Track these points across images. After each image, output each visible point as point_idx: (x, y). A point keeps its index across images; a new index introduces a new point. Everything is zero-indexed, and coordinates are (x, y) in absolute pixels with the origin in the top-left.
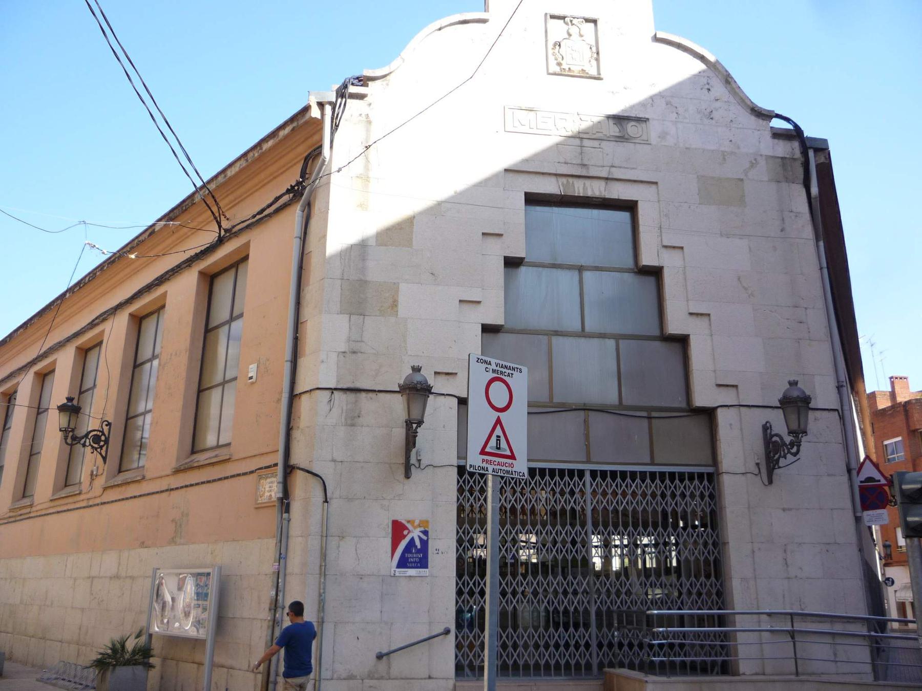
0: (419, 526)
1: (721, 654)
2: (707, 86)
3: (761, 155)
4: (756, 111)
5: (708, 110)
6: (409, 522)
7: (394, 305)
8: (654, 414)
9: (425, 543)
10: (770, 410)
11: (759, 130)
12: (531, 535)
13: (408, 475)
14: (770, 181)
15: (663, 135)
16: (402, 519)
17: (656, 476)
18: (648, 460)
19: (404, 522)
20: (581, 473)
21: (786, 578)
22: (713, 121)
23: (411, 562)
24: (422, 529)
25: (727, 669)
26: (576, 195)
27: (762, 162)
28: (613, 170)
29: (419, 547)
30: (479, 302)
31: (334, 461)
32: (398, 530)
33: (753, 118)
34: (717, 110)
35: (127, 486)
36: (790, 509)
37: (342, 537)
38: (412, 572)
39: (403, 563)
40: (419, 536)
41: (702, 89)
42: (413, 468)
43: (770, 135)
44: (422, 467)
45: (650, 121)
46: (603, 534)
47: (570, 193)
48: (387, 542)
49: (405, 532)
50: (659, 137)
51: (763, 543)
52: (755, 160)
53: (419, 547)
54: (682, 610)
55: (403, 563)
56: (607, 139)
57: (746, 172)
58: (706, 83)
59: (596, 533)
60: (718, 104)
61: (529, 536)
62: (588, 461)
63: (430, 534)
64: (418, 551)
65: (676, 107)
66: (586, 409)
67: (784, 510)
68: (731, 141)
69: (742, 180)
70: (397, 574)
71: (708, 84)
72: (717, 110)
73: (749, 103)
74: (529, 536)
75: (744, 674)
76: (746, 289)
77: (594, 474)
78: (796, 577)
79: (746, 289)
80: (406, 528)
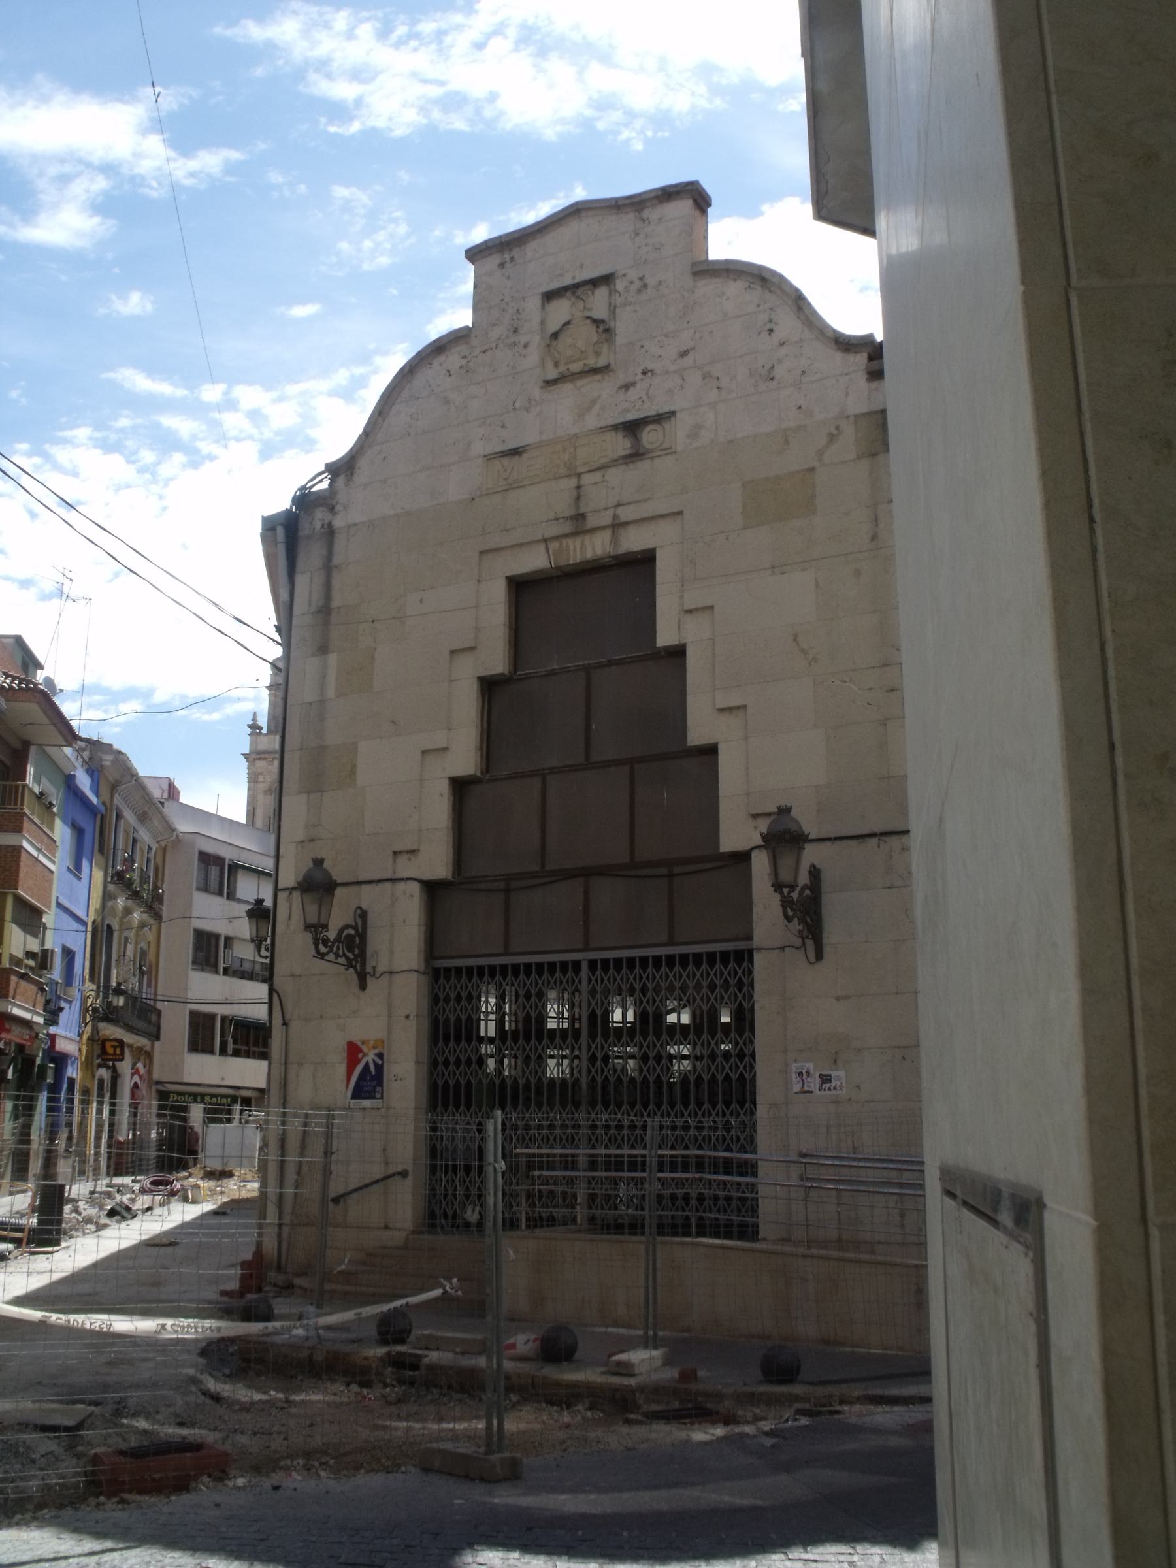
0: (374, 1047)
1: (725, 1211)
2: (768, 326)
3: (848, 417)
4: (841, 343)
5: (767, 367)
6: (363, 1043)
7: (353, 772)
8: (677, 870)
9: (379, 1068)
10: (828, 843)
11: (847, 374)
12: (682, 1047)
13: (363, 987)
14: (859, 458)
15: (694, 434)
16: (356, 1038)
17: (688, 960)
18: (664, 938)
19: (359, 1044)
20: (577, 965)
21: (834, 1102)
22: (775, 383)
23: (366, 1092)
24: (376, 1051)
25: (748, 1232)
26: (571, 562)
27: (849, 431)
28: (620, 511)
29: (374, 1073)
30: (446, 749)
31: (293, 975)
32: (353, 1051)
33: (839, 356)
34: (780, 361)
35: (861, 840)
36: (846, 997)
37: (301, 1064)
38: (367, 1103)
39: (358, 1093)
40: (374, 1061)
41: (759, 333)
42: (368, 977)
43: (866, 376)
44: (377, 975)
45: (678, 415)
46: (512, 1049)
47: (563, 563)
48: (342, 1069)
49: (360, 1055)
50: (688, 436)
51: (802, 1051)
52: (837, 428)
53: (374, 1073)
54: (746, 1152)
55: (358, 1093)
56: (614, 463)
57: (820, 454)
58: (767, 319)
59: (564, 1047)
60: (784, 351)
61: (679, 1049)
62: (586, 949)
63: (385, 1057)
64: (373, 1078)
65: (718, 378)
66: (587, 873)
67: (838, 999)
68: (800, 408)
69: (812, 470)
70: (352, 1106)
71: (770, 321)
72: (780, 361)
73: (829, 334)
74: (679, 1049)
75: (765, 1239)
76: (803, 651)
77: (593, 964)
78: (850, 1099)
79: (803, 651)
80: (361, 1051)
